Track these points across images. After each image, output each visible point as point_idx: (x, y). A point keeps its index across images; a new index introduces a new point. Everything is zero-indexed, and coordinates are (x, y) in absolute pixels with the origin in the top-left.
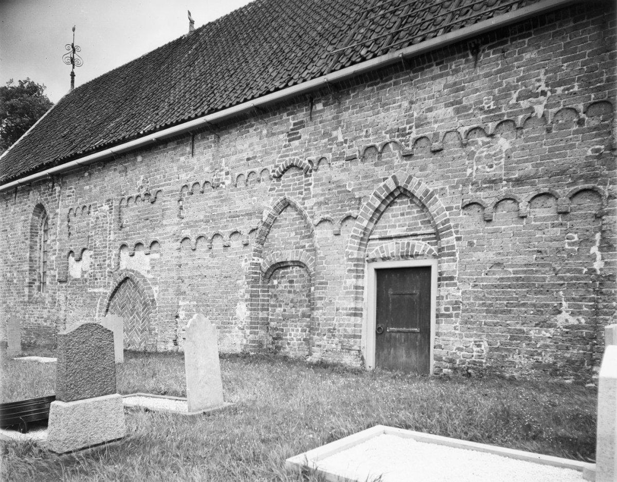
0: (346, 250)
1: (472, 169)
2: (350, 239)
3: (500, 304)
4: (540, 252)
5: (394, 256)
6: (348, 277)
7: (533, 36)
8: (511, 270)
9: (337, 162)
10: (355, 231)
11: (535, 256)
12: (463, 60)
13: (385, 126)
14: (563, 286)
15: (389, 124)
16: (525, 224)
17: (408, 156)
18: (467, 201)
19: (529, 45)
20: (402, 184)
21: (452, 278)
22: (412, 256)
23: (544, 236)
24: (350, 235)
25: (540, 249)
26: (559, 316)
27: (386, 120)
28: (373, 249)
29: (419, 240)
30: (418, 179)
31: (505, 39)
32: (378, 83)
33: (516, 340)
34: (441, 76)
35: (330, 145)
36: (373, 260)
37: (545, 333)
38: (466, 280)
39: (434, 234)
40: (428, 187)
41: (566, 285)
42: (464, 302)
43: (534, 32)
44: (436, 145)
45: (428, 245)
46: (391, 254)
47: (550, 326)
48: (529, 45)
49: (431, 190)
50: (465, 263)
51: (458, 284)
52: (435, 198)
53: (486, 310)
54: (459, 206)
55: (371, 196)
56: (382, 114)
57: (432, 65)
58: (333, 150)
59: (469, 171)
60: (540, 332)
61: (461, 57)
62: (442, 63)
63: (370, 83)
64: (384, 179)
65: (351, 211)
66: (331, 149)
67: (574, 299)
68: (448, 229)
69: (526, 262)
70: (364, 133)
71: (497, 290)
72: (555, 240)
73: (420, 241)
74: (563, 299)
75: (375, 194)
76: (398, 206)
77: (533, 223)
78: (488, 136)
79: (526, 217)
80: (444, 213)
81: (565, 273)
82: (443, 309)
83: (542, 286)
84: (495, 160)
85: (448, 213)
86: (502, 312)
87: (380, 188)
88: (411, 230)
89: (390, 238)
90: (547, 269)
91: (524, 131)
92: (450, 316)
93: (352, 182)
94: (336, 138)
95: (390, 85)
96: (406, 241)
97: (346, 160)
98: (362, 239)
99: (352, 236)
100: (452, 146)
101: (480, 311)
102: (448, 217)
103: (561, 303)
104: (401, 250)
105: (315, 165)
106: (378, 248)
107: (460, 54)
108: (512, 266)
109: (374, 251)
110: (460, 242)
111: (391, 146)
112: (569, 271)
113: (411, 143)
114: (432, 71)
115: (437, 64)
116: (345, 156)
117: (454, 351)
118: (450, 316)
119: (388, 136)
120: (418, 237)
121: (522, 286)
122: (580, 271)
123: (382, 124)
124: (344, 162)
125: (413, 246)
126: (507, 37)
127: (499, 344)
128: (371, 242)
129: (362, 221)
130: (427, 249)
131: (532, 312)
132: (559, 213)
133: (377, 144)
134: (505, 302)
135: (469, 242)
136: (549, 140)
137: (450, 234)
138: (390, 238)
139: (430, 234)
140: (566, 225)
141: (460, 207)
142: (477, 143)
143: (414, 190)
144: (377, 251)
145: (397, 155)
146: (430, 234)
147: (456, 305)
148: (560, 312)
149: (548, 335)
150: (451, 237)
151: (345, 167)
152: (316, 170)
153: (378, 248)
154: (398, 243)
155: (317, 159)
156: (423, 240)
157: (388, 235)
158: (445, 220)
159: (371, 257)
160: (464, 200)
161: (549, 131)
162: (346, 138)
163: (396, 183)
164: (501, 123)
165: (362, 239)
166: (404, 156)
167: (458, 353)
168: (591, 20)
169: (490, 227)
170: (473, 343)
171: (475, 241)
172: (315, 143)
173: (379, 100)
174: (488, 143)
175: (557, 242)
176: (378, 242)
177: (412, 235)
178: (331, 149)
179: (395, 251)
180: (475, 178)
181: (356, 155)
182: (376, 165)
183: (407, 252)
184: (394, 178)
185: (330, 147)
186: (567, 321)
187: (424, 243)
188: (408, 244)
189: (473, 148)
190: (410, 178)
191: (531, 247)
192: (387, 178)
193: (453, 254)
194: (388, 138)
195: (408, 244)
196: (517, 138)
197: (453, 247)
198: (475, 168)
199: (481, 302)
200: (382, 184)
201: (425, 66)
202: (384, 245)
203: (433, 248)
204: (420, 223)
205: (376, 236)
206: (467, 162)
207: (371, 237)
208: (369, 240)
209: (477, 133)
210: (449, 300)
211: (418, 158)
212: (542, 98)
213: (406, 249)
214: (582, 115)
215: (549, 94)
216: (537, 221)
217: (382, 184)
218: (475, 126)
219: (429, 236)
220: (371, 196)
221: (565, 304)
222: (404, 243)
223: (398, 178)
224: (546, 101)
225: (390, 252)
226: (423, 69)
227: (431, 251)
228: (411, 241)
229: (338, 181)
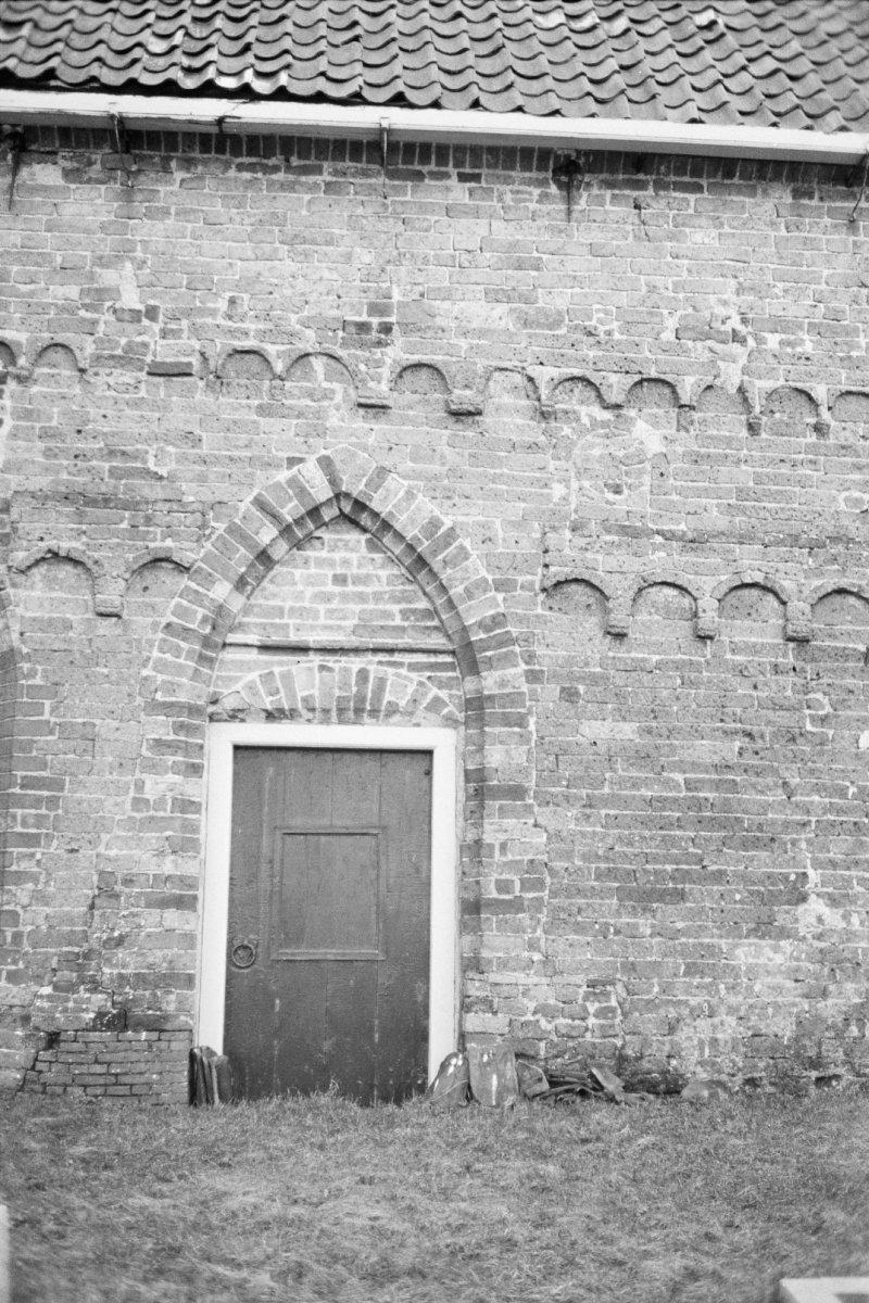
0: (145, 672)
1: (568, 487)
2: (161, 635)
3: (656, 872)
4: (749, 735)
5: (313, 710)
6: (152, 767)
7: (706, 194)
8: (679, 777)
9: (117, 372)
10: (180, 612)
11: (737, 744)
12: (536, 192)
13: (298, 301)
14: (808, 829)
15: (312, 298)
16: (709, 656)
17: (376, 409)
18: (558, 572)
19: (698, 213)
20: (357, 489)
21: (517, 792)
22: (374, 713)
23: (754, 693)
24: (164, 622)
25: (748, 727)
26: (801, 908)
27: (300, 283)
28: (237, 679)
29: (401, 664)
30: (406, 483)
31: (641, 176)
32: (276, 169)
33: (703, 974)
34: (466, 212)
35: (87, 307)
36: (235, 715)
37: (771, 955)
38: (560, 798)
39: (453, 653)
40: (437, 512)
41: (813, 825)
42: (559, 865)
43: (709, 185)
44: (463, 396)
45: (429, 684)
46: (305, 700)
47: (784, 933)
48: (698, 213)
49: (448, 523)
50: (556, 749)
51: (536, 809)
52: (462, 548)
53: (617, 888)
54: (532, 583)
55: (243, 507)
56: (289, 266)
57: (446, 176)
58: (101, 328)
59: (558, 490)
60: (759, 952)
61: (530, 182)
62: (476, 178)
63: (246, 160)
64: (292, 462)
65: (169, 543)
66: (94, 323)
67: (833, 864)
68: (501, 644)
69: (716, 759)
70: (222, 305)
71: (647, 833)
72: (781, 708)
73: (403, 671)
74: (809, 861)
75: (260, 503)
76: (324, 554)
77: (729, 656)
78: (607, 407)
79: (711, 638)
80: (489, 595)
81: (808, 795)
82: (492, 886)
83: (760, 827)
84: (627, 473)
85: (500, 596)
86: (662, 896)
87: (278, 485)
88: (374, 631)
89: (303, 649)
90: (770, 780)
91: (696, 416)
92: (516, 906)
93: (170, 449)
94: (114, 293)
95: (314, 187)
96: (355, 663)
97: (149, 374)
98: (206, 642)
99: (168, 625)
100: (507, 415)
101: (601, 894)
102: (501, 610)
103: (805, 874)
104: (337, 693)
105: (22, 361)
106: (254, 676)
107: (527, 174)
108: (680, 767)
109: (238, 686)
110: (538, 687)
111: (318, 364)
112: (817, 789)
113: (386, 372)
114: (448, 189)
115: (463, 178)
116: (149, 359)
117: (529, 1017)
118: (516, 906)
119: (310, 334)
120: (397, 657)
121: (713, 823)
122: (842, 792)
123: (288, 292)
124: (143, 375)
125: (381, 682)
126: (646, 174)
127: (656, 989)
128: (229, 655)
129: (209, 580)
130: (424, 695)
131: (738, 897)
132: (790, 639)
133: (271, 350)
134: (669, 868)
135: (563, 690)
136: (753, 453)
137: (508, 660)
138: (303, 649)
139: (435, 652)
140: (803, 670)
141: (537, 587)
142: (578, 420)
143: (391, 513)
144: (251, 687)
145: (339, 398)
146: (435, 652)
147: (533, 875)
148: (803, 899)
149: (779, 959)
150: (512, 671)
151: (143, 393)
152: (20, 379)
153: (254, 676)
154: (330, 670)
155: (31, 342)
156: (413, 667)
157: (294, 638)
158: (493, 618)
159: (229, 703)
160: (552, 569)
161: (752, 428)
162: (152, 302)
163: (333, 482)
164: (640, 382)
165: (206, 642)
166: (360, 405)
167: (543, 1023)
168: (826, 204)
169: (621, 653)
170: (585, 988)
171: (581, 689)
172: (24, 288)
173: (278, 220)
174: (605, 424)
175: (787, 714)
176: (254, 655)
177: (375, 650)
178: (94, 323)
179: (316, 692)
180: (576, 511)
181: (189, 364)
182: (262, 410)
183: (361, 699)
184: (326, 464)
185: (88, 315)
186: (820, 920)
187: (414, 675)
188: (363, 675)
189: (567, 431)
190: (382, 472)
191: (727, 719)
192: (301, 460)
193: (521, 722)
194: (309, 340)
195: (363, 675)
196: (678, 430)
197: (515, 698)
198: (575, 485)
199: (603, 865)
200: (283, 475)
201: (425, 169)
202: (277, 670)
203: (443, 694)
204: (322, 613)
205: (253, 639)
206: (552, 465)
207: (231, 638)
208: (225, 645)
209: (576, 391)
210: (510, 857)
211: (404, 420)
212: (736, 348)
213: (354, 689)
214: (826, 415)
215: (751, 342)
216: (739, 654)
217: (283, 475)
218: (576, 372)
219: (432, 659)
220: (243, 507)
221: (814, 875)
222: (346, 670)
223: (338, 465)
224: (745, 357)
225: (300, 694)
226: (419, 176)
227: (437, 704)
228: (372, 668)
229: (114, 434)
